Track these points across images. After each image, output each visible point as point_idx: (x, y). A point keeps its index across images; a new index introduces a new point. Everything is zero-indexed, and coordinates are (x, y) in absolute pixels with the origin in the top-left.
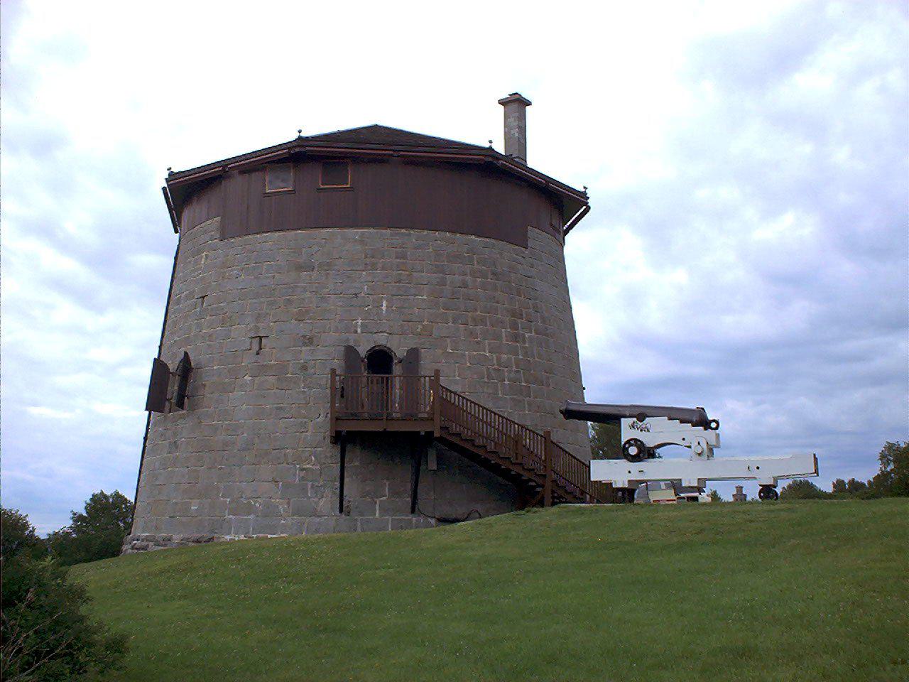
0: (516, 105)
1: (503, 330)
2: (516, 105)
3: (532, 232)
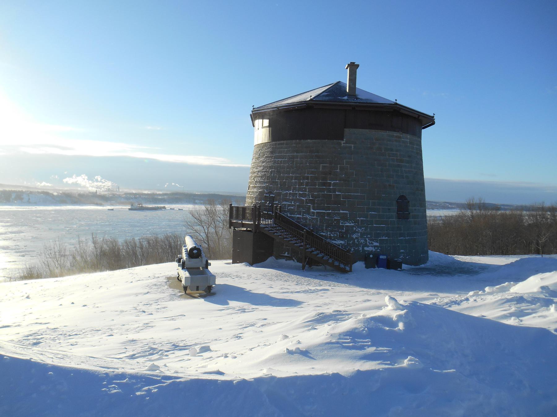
2: (353, 67)
3: (346, 130)
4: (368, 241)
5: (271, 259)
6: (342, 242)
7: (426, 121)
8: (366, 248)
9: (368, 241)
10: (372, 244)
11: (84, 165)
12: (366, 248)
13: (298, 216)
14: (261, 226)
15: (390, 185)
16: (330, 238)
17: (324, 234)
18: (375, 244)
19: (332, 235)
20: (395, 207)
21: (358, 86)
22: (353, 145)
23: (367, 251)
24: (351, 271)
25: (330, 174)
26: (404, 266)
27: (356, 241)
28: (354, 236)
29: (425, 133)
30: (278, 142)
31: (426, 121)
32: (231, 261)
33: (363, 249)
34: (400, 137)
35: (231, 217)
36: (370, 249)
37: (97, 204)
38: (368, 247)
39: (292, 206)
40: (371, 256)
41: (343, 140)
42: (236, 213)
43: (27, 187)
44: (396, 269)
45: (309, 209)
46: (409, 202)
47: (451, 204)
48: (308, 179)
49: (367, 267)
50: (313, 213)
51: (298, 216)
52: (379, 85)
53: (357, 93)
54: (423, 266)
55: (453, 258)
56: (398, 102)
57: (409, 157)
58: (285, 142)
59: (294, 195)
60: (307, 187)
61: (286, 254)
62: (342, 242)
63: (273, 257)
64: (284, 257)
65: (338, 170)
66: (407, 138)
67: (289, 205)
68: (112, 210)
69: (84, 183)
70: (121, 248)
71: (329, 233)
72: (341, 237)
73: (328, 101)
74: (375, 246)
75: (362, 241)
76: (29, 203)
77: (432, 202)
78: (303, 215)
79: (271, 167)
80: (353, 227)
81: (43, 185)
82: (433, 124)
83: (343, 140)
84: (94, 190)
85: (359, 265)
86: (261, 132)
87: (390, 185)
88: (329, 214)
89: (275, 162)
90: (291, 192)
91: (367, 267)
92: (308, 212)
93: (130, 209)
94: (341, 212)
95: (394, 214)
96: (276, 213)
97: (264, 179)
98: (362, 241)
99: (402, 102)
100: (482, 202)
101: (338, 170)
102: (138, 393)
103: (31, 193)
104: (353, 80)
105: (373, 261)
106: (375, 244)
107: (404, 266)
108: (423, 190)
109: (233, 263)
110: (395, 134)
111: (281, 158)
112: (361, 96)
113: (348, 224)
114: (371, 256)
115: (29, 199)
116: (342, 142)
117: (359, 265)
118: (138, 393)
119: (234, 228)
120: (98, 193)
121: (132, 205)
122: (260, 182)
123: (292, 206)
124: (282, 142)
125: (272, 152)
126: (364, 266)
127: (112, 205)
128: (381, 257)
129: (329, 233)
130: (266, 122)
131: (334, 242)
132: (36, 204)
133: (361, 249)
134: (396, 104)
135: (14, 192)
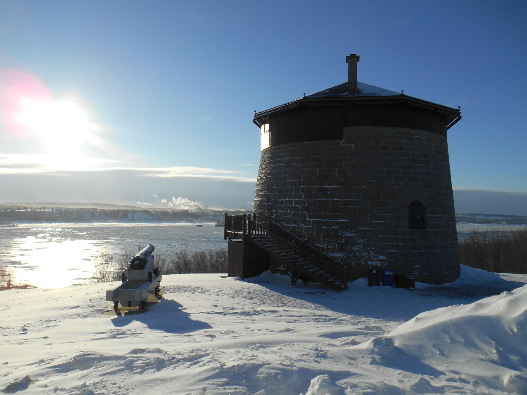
2: (353, 60)
4: (372, 253)
5: (266, 274)
6: (341, 255)
7: (447, 117)
8: (370, 263)
9: (372, 253)
10: (377, 257)
11: (181, 186)
12: (370, 263)
13: (293, 225)
14: (252, 236)
16: (328, 250)
17: (321, 246)
18: (381, 257)
19: (330, 247)
21: (359, 80)
22: (353, 145)
23: (371, 265)
26: (418, 285)
27: (357, 253)
28: (355, 248)
30: (276, 147)
31: (447, 117)
32: (227, 275)
33: (366, 262)
36: (375, 263)
37: (189, 221)
38: (372, 260)
39: (288, 214)
40: (374, 272)
41: (342, 140)
42: (231, 222)
43: (132, 207)
44: (407, 287)
45: (305, 218)
46: (425, 208)
48: (303, 185)
49: (370, 284)
50: (309, 222)
51: (293, 225)
52: (380, 78)
53: (358, 87)
54: (447, 285)
55: (498, 277)
56: (404, 93)
58: (282, 146)
59: (290, 202)
60: (303, 194)
61: (281, 268)
62: (341, 255)
63: (269, 271)
64: (278, 271)
65: (336, 174)
67: (285, 214)
68: (201, 226)
69: (182, 204)
71: (326, 245)
72: (340, 249)
73: (323, 98)
74: (380, 261)
75: (365, 254)
76: (133, 220)
78: (298, 225)
79: (269, 174)
80: (354, 237)
81: (145, 205)
83: (342, 140)
84: (186, 208)
86: (265, 138)
88: (326, 223)
89: (273, 167)
90: (287, 199)
91: (370, 284)
92: (304, 221)
93: (216, 226)
94: (340, 220)
96: (271, 222)
97: (264, 187)
98: (365, 254)
99: (408, 93)
101: (336, 174)
102: (515, 330)
103: (135, 211)
104: (353, 73)
105: (376, 279)
106: (381, 257)
107: (418, 285)
109: (228, 276)
110: (406, 130)
111: (280, 163)
112: (366, 92)
113: (348, 235)
114: (374, 272)
116: (341, 142)
117: (362, 282)
118: (515, 330)
119: (229, 238)
120: (189, 212)
121: (218, 222)
122: (261, 190)
123: (288, 214)
124: (280, 146)
125: (271, 158)
126: (366, 283)
127: (201, 221)
128: (387, 273)
129: (326, 245)
130: (267, 126)
131: (332, 254)
132: (138, 221)
133: (363, 263)
134: (403, 95)
135: (122, 211)
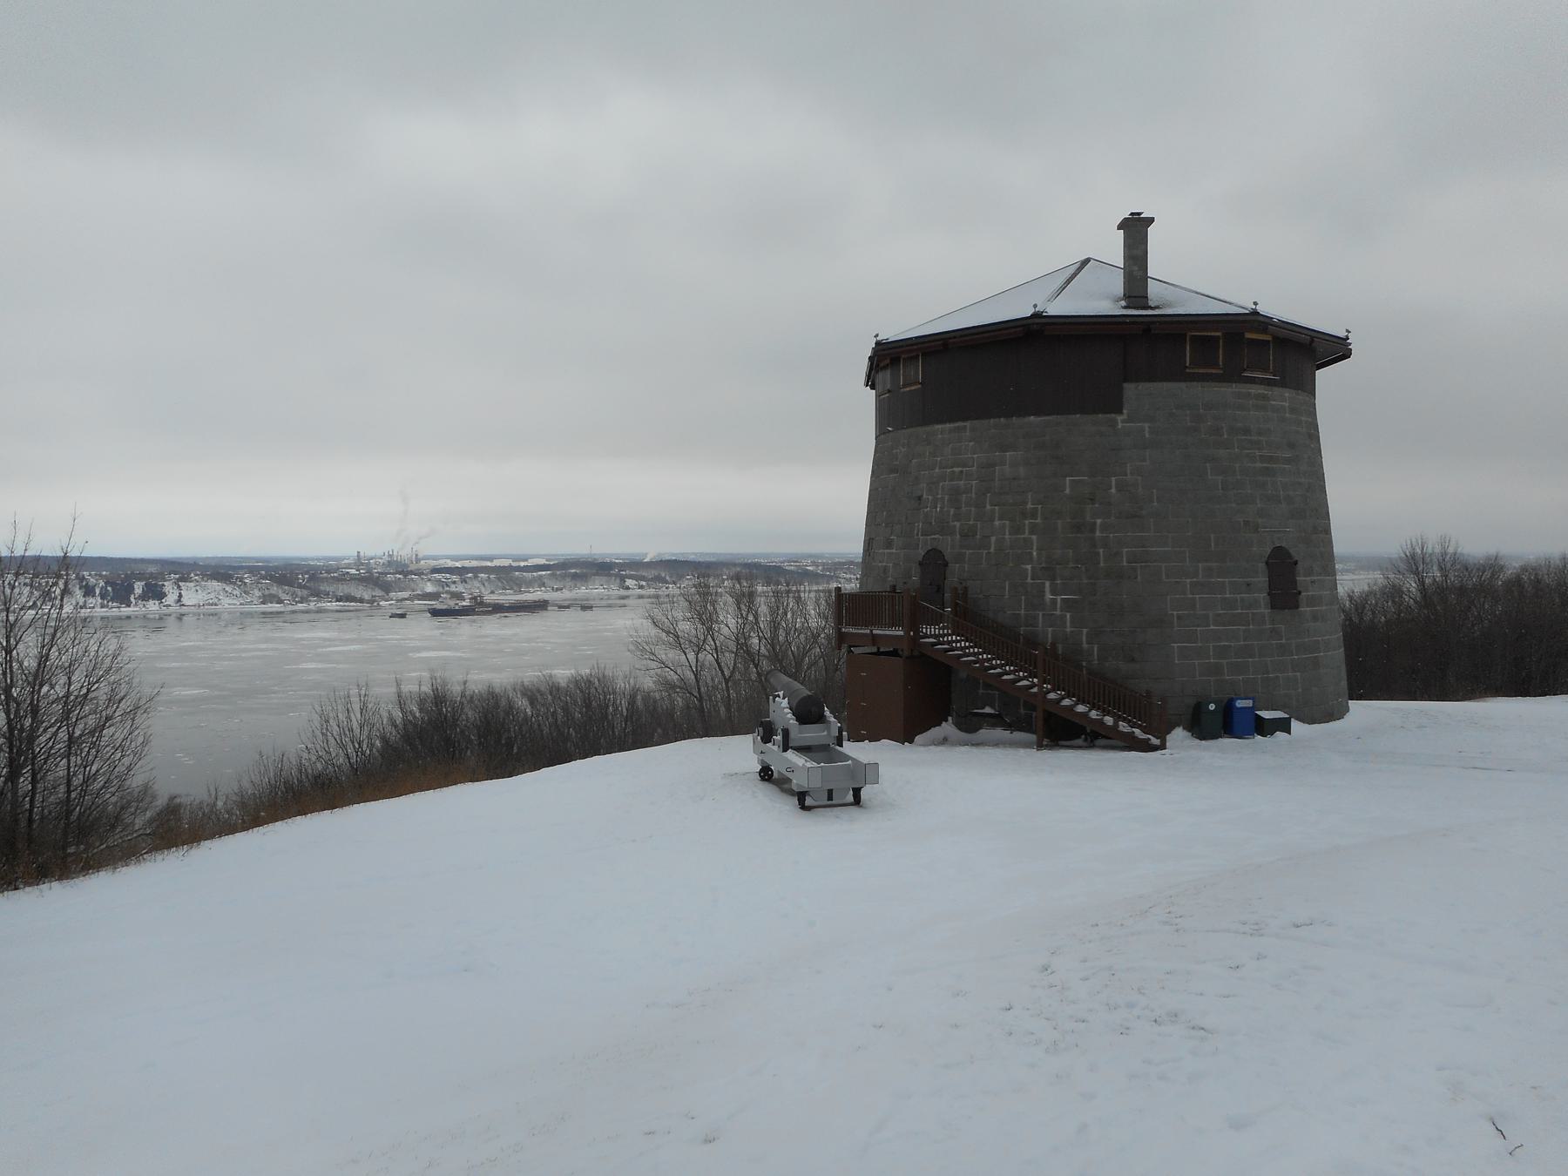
0: (1135, 228)
1: (1059, 522)
2: (1135, 228)
3: (1130, 390)
15: (1246, 523)
20: (1262, 579)
22: (1146, 425)
24: (1163, 747)
25: (1092, 500)
29: (1325, 378)
34: (1265, 397)
35: (839, 620)
41: (1120, 412)
47: (506, 575)
57: (1292, 446)
58: (968, 424)
61: (988, 710)
66: (1283, 398)
70: (657, 696)
77: (143, 561)
82: (1346, 355)
83: (1120, 412)
85: (1178, 735)
87: (1246, 523)
95: (1262, 596)
100: (1451, 550)
108: (1327, 531)
114: (1212, 707)
115: (180, 595)
116: (1119, 418)
128: (1240, 704)
134: (1255, 313)
